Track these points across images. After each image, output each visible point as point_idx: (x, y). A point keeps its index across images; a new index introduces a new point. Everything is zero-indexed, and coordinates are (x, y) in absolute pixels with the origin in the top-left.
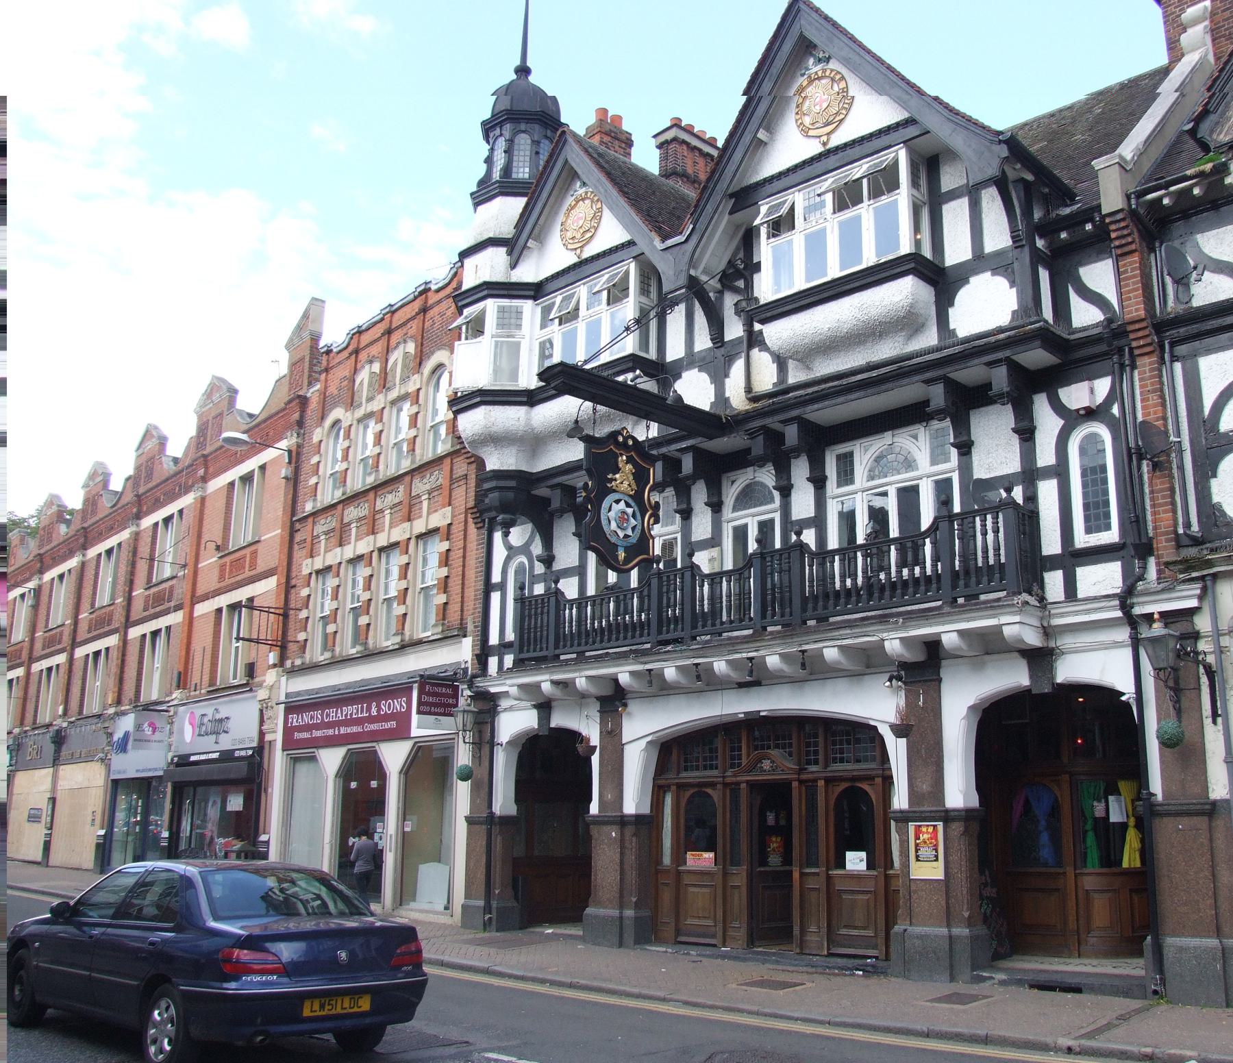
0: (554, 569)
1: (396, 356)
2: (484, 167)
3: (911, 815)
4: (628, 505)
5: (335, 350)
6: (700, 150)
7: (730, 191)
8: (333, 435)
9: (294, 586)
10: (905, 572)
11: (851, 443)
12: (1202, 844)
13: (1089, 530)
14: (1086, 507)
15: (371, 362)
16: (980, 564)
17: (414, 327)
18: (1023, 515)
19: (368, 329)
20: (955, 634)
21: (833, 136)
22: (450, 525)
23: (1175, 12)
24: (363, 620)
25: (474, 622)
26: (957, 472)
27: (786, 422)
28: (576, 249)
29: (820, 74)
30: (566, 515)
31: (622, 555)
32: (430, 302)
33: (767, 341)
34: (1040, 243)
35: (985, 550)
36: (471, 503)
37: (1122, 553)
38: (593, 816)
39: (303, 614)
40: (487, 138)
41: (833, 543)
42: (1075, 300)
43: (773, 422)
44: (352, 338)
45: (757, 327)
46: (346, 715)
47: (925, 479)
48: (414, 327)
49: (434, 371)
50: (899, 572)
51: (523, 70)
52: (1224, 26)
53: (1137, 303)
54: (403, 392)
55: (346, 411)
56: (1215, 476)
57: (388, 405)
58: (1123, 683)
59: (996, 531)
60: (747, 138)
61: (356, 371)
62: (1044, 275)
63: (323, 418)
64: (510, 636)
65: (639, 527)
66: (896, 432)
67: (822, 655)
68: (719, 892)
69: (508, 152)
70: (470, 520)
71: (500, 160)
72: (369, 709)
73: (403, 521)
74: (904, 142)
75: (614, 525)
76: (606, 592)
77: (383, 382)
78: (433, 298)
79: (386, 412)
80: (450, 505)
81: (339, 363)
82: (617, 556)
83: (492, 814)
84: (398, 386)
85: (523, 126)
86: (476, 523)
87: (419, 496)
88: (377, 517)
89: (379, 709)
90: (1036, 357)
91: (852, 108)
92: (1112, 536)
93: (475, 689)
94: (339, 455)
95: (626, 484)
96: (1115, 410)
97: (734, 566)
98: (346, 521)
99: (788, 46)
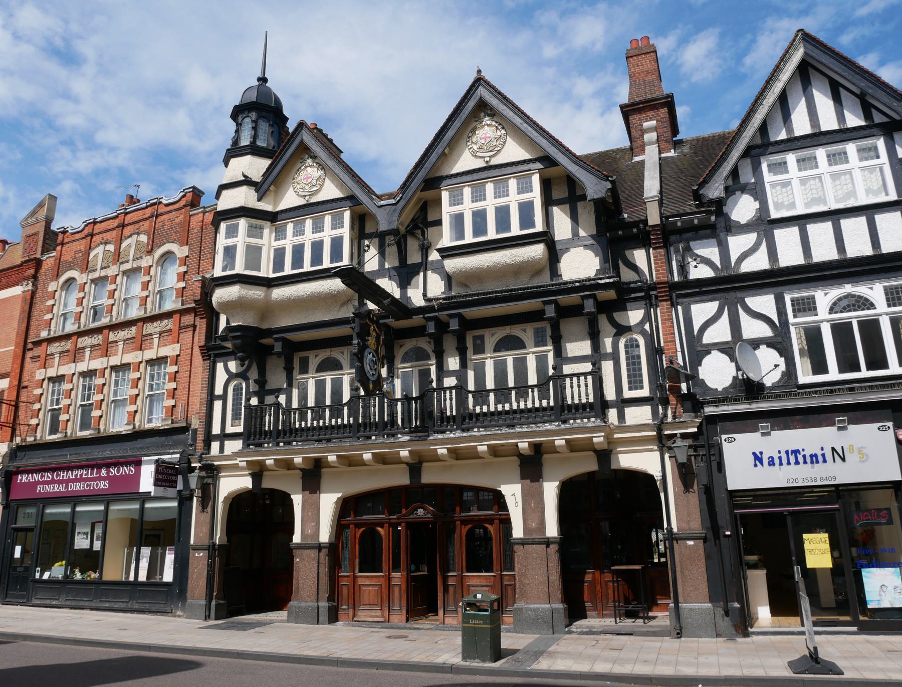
0: (266, 388)
5: (70, 231)
8: (65, 287)
9: (26, 387)
10: (333, 421)
11: (308, 352)
13: (630, 389)
14: (629, 376)
19: (101, 222)
20: (564, 441)
22: (178, 356)
26: (435, 366)
27: (451, 316)
28: (305, 196)
29: (311, 164)
35: (573, 397)
37: (651, 402)
39: (37, 406)
41: (295, 405)
43: (443, 314)
44: (86, 226)
51: (263, 80)
53: (663, 273)
54: (135, 266)
56: (701, 365)
57: (89, 281)
58: (655, 471)
59: (451, 399)
61: (90, 248)
63: (58, 276)
66: (333, 349)
67: (554, 443)
68: (385, 591)
69: (255, 128)
72: (99, 472)
77: (117, 257)
83: (214, 544)
85: (264, 114)
91: (506, 145)
92: (645, 392)
93: (204, 462)
99: (471, 104)
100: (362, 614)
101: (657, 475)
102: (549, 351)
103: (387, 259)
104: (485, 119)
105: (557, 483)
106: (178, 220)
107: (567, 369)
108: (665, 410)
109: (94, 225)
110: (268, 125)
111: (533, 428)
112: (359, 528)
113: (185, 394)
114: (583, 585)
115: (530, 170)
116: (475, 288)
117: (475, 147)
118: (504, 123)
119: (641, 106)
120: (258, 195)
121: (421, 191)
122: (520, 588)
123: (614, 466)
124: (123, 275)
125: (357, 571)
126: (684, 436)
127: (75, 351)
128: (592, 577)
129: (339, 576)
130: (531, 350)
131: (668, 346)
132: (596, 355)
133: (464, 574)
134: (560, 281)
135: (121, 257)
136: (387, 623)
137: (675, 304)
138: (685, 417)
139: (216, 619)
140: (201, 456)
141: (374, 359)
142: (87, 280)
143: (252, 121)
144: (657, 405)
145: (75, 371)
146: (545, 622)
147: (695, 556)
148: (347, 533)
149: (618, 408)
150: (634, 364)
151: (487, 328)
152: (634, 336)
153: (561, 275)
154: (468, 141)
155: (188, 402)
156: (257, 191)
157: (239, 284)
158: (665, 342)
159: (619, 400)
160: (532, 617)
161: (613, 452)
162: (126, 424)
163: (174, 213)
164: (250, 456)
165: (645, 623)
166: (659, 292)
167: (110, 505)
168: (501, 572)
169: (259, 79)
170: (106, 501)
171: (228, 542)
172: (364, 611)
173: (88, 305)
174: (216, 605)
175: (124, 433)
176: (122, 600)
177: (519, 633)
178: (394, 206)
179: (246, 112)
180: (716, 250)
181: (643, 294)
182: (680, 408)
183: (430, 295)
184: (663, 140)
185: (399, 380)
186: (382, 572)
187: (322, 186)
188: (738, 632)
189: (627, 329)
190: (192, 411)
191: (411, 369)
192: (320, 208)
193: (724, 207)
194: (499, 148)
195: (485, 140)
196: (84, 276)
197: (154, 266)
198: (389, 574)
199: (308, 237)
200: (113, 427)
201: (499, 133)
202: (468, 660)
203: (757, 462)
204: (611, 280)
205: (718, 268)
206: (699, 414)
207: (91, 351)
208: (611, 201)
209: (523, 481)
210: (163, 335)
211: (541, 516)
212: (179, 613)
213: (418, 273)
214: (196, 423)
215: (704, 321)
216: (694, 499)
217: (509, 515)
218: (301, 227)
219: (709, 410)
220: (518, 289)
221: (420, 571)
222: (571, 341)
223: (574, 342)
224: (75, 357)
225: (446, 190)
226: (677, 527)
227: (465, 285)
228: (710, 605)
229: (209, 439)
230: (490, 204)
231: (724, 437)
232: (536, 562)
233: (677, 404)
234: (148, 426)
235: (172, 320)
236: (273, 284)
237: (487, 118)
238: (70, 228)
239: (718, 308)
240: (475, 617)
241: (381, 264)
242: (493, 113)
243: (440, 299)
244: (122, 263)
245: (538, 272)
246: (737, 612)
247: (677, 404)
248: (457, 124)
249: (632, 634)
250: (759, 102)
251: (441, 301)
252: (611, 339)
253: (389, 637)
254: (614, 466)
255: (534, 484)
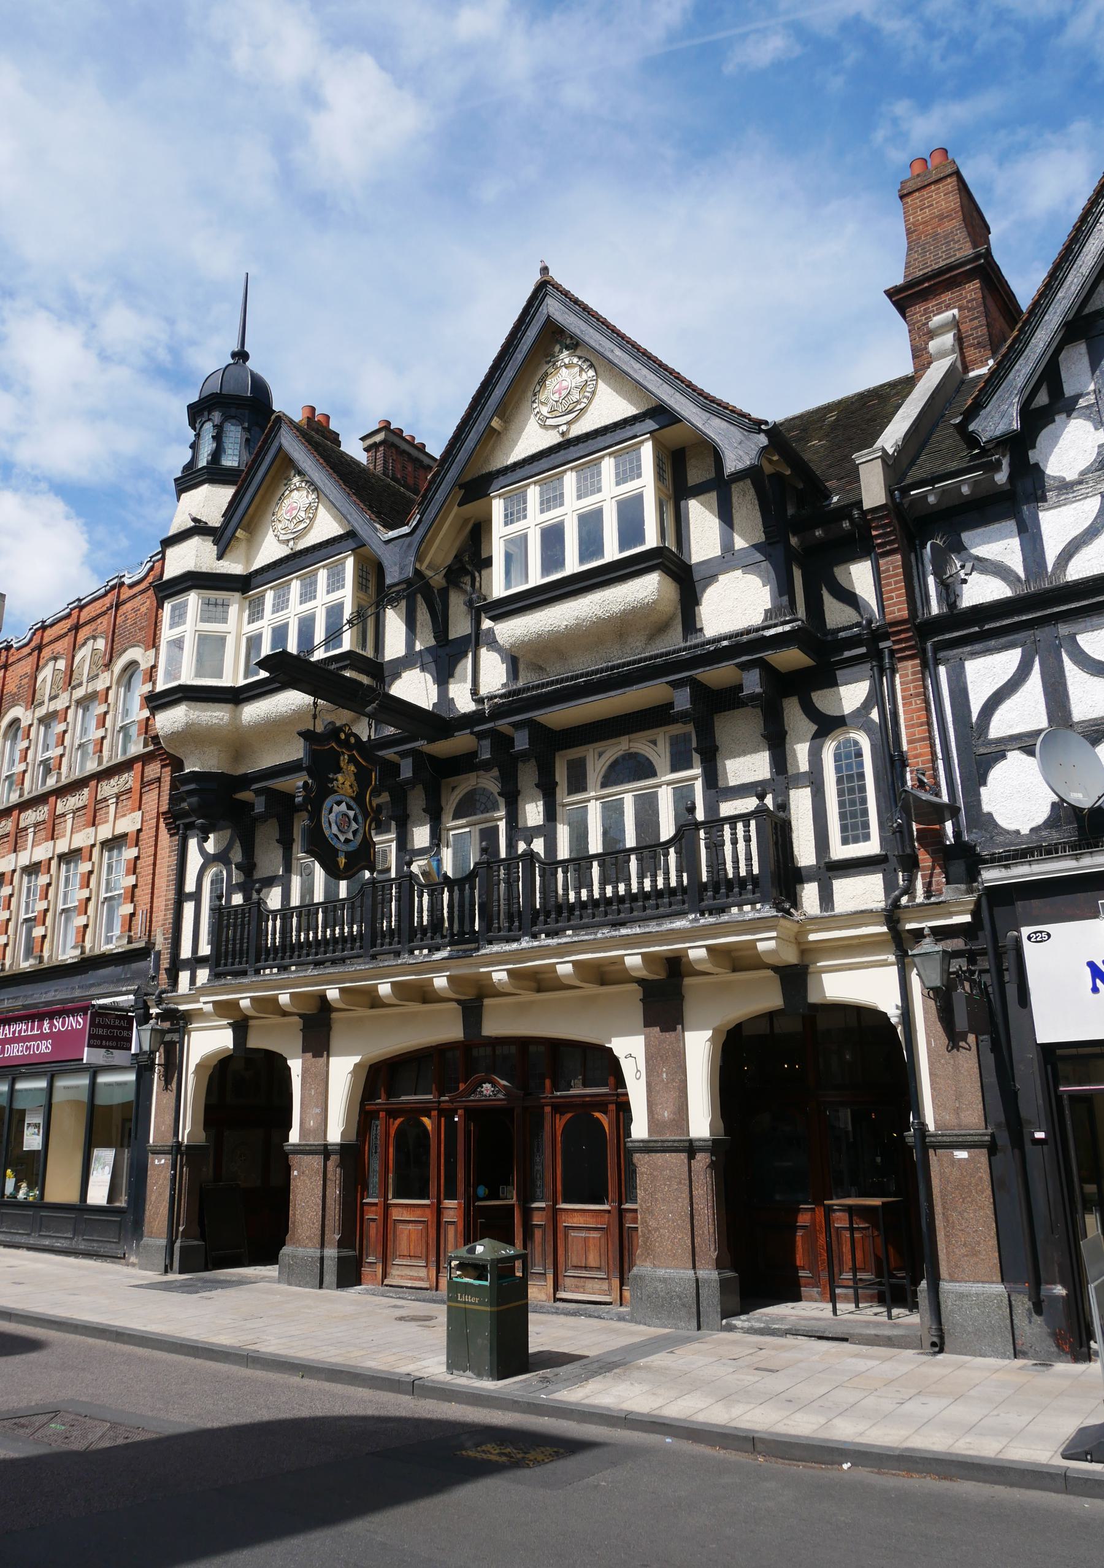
1: (83, 653)
2: (190, 452)
3: (652, 1144)
4: (349, 808)
5: (15, 646)
6: (409, 454)
7: (460, 482)
8: (11, 734)
12: (981, 1178)
13: (845, 841)
14: (842, 816)
15: (55, 659)
16: (730, 876)
17: (104, 623)
18: (776, 823)
19: (52, 625)
20: (704, 950)
21: (573, 427)
22: (139, 831)
23: (921, 320)
24: (38, 932)
25: (164, 934)
26: (700, 779)
28: (288, 541)
29: (297, 484)
30: (270, 821)
31: (342, 861)
32: (123, 597)
33: (498, 638)
34: (794, 541)
35: (736, 861)
36: (164, 808)
37: (883, 866)
38: (293, 1145)
40: (192, 424)
41: (563, 852)
42: (828, 599)
43: (502, 725)
44: (34, 634)
45: (487, 624)
46: (14, 1032)
47: (664, 787)
48: (104, 623)
49: (125, 669)
50: (603, 890)
51: (241, 356)
52: (972, 334)
53: (900, 603)
54: (90, 690)
55: (26, 710)
57: (35, 722)
58: (889, 1004)
59: (748, 840)
60: (480, 427)
61: (38, 668)
62: (797, 574)
64: (205, 950)
65: (361, 831)
66: (633, 736)
69: (218, 438)
70: (162, 825)
71: (207, 448)
72: (40, 1027)
73: (86, 826)
74: (650, 433)
75: (335, 830)
76: (331, 904)
77: (69, 679)
78: (126, 593)
79: (71, 712)
80: (140, 809)
81: (19, 660)
82: (337, 863)
84: (85, 684)
85: (233, 411)
86: (169, 830)
87: (105, 800)
88: (57, 821)
89: (52, 1025)
90: (792, 658)
92: (872, 847)
93: (164, 1006)
94: (17, 756)
95: (348, 783)
96: (875, 715)
97: (604, 848)
98: (22, 825)
99: (532, 333)
100: (398, 1273)
101: (893, 1014)
102: (696, 779)
103: (418, 635)
104: (561, 356)
105: (709, 1033)
106: (143, 609)
107: (727, 809)
108: (911, 881)
109: (43, 632)
110: (239, 428)
111: (653, 927)
112: (395, 1119)
113: (147, 894)
114: (795, 1236)
115: (635, 437)
116: (556, 672)
117: (545, 410)
118: (595, 360)
119: (926, 285)
120: (218, 550)
121: (460, 505)
122: (643, 1236)
123: (813, 998)
124: (77, 707)
125: (390, 1197)
126: (940, 933)
127: (17, 833)
128: (812, 1219)
129: (363, 1204)
130: (663, 779)
131: (915, 749)
132: (781, 777)
133: (557, 1207)
134: (698, 641)
135: (74, 677)
136: (434, 1292)
137: (931, 662)
138: (948, 893)
139: (181, 1272)
140: (159, 996)
141: (351, 813)
142: (33, 720)
143: (214, 426)
144: (895, 870)
145: (16, 866)
146: (684, 1305)
147: (970, 1184)
148: (377, 1126)
149: (819, 881)
150: (851, 790)
151: (589, 743)
152: (851, 735)
153: (701, 630)
154: (534, 402)
155: (151, 907)
156: (215, 543)
157: (185, 703)
158: (909, 742)
159: (822, 865)
160: (662, 1294)
161: (810, 970)
162: (72, 948)
163: (139, 597)
164: (217, 994)
165: (890, 1317)
166: (895, 642)
167: (55, 1079)
168: (620, 1203)
169: (234, 355)
170: (49, 1074)
171: (207, 1142)
172: (400, 1268)
173: (35, 760)
174: (181, 1247)
175: (69, 961)
176: (65, 1235)
177: (640, 1323)
178: (409, 538)
179: (206, 413)
180: (1015, 543)
181: (863, 650)
182: (940, 874)
183: (484, 691)
184: (972, 345)
185: (450, 850)
186: (428, 1199)
187: (312, 520)
188: (1063, 1350)
189: (838, 722)
190: (157, 922)
191: (467, 830)
192: (310, 558)
193: (1030, 453)
194: (583, 405)
195: (560, 394)
196: (29, 713)
197: (114, 687)
198: (439, 1202)
199: (295, 610)
200: (64, 952)
201: (584, 376)
202: (455, 1372)
203: (1098, 981)
204: (787, 628)
205: (1018, 579)
206: (975, 884)
207: (35, 833)
208: (788, 472)
209: (648, 1030)
210: (121, 798)
211: (680, 1097)
212: (133, 1259)
213: (465, 655)
214: (161, 942)
215: (990, 693)
216: (967, 1061)
217: (627, 1095)
218: (631, 462)
219: (991, 876)
220: (624, 665)
221: (498, 1198)
222: (734, 755)
223: (739, 756)
224: (16, 843)
225: (499, 496)
226: (935, 1122)
227: (540, 669)
228: (999, 1288)
229: (176, 965)
230: (570, 512)
231: (1026, 931)
232: (669, 1186)
233: (933, 868)
234: (106, 948)
235: (132, 774)
236: (241, 697)
237: (566, 353)
238: (15, 640)
239: (1021, 662)
240: (467, 1289)
241: (410, 644)
242: (574, 344)
243: (496, 697)
244: (74, 688)
245: (661, 628)
246: (1060, 1306)
247: (933, 868)
248: (509, 373)
249: (845, 1340)
250: (1091, 220)
251: (496, 700)
252: (808, 744)
253: (401, 1319)
254: (813, 998)
255: (667, 1035)
